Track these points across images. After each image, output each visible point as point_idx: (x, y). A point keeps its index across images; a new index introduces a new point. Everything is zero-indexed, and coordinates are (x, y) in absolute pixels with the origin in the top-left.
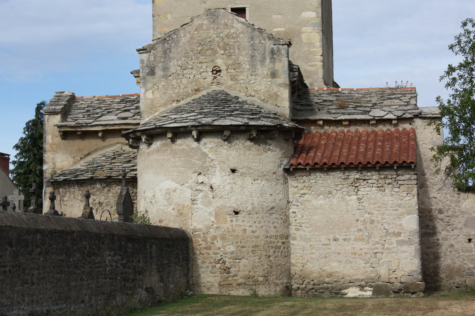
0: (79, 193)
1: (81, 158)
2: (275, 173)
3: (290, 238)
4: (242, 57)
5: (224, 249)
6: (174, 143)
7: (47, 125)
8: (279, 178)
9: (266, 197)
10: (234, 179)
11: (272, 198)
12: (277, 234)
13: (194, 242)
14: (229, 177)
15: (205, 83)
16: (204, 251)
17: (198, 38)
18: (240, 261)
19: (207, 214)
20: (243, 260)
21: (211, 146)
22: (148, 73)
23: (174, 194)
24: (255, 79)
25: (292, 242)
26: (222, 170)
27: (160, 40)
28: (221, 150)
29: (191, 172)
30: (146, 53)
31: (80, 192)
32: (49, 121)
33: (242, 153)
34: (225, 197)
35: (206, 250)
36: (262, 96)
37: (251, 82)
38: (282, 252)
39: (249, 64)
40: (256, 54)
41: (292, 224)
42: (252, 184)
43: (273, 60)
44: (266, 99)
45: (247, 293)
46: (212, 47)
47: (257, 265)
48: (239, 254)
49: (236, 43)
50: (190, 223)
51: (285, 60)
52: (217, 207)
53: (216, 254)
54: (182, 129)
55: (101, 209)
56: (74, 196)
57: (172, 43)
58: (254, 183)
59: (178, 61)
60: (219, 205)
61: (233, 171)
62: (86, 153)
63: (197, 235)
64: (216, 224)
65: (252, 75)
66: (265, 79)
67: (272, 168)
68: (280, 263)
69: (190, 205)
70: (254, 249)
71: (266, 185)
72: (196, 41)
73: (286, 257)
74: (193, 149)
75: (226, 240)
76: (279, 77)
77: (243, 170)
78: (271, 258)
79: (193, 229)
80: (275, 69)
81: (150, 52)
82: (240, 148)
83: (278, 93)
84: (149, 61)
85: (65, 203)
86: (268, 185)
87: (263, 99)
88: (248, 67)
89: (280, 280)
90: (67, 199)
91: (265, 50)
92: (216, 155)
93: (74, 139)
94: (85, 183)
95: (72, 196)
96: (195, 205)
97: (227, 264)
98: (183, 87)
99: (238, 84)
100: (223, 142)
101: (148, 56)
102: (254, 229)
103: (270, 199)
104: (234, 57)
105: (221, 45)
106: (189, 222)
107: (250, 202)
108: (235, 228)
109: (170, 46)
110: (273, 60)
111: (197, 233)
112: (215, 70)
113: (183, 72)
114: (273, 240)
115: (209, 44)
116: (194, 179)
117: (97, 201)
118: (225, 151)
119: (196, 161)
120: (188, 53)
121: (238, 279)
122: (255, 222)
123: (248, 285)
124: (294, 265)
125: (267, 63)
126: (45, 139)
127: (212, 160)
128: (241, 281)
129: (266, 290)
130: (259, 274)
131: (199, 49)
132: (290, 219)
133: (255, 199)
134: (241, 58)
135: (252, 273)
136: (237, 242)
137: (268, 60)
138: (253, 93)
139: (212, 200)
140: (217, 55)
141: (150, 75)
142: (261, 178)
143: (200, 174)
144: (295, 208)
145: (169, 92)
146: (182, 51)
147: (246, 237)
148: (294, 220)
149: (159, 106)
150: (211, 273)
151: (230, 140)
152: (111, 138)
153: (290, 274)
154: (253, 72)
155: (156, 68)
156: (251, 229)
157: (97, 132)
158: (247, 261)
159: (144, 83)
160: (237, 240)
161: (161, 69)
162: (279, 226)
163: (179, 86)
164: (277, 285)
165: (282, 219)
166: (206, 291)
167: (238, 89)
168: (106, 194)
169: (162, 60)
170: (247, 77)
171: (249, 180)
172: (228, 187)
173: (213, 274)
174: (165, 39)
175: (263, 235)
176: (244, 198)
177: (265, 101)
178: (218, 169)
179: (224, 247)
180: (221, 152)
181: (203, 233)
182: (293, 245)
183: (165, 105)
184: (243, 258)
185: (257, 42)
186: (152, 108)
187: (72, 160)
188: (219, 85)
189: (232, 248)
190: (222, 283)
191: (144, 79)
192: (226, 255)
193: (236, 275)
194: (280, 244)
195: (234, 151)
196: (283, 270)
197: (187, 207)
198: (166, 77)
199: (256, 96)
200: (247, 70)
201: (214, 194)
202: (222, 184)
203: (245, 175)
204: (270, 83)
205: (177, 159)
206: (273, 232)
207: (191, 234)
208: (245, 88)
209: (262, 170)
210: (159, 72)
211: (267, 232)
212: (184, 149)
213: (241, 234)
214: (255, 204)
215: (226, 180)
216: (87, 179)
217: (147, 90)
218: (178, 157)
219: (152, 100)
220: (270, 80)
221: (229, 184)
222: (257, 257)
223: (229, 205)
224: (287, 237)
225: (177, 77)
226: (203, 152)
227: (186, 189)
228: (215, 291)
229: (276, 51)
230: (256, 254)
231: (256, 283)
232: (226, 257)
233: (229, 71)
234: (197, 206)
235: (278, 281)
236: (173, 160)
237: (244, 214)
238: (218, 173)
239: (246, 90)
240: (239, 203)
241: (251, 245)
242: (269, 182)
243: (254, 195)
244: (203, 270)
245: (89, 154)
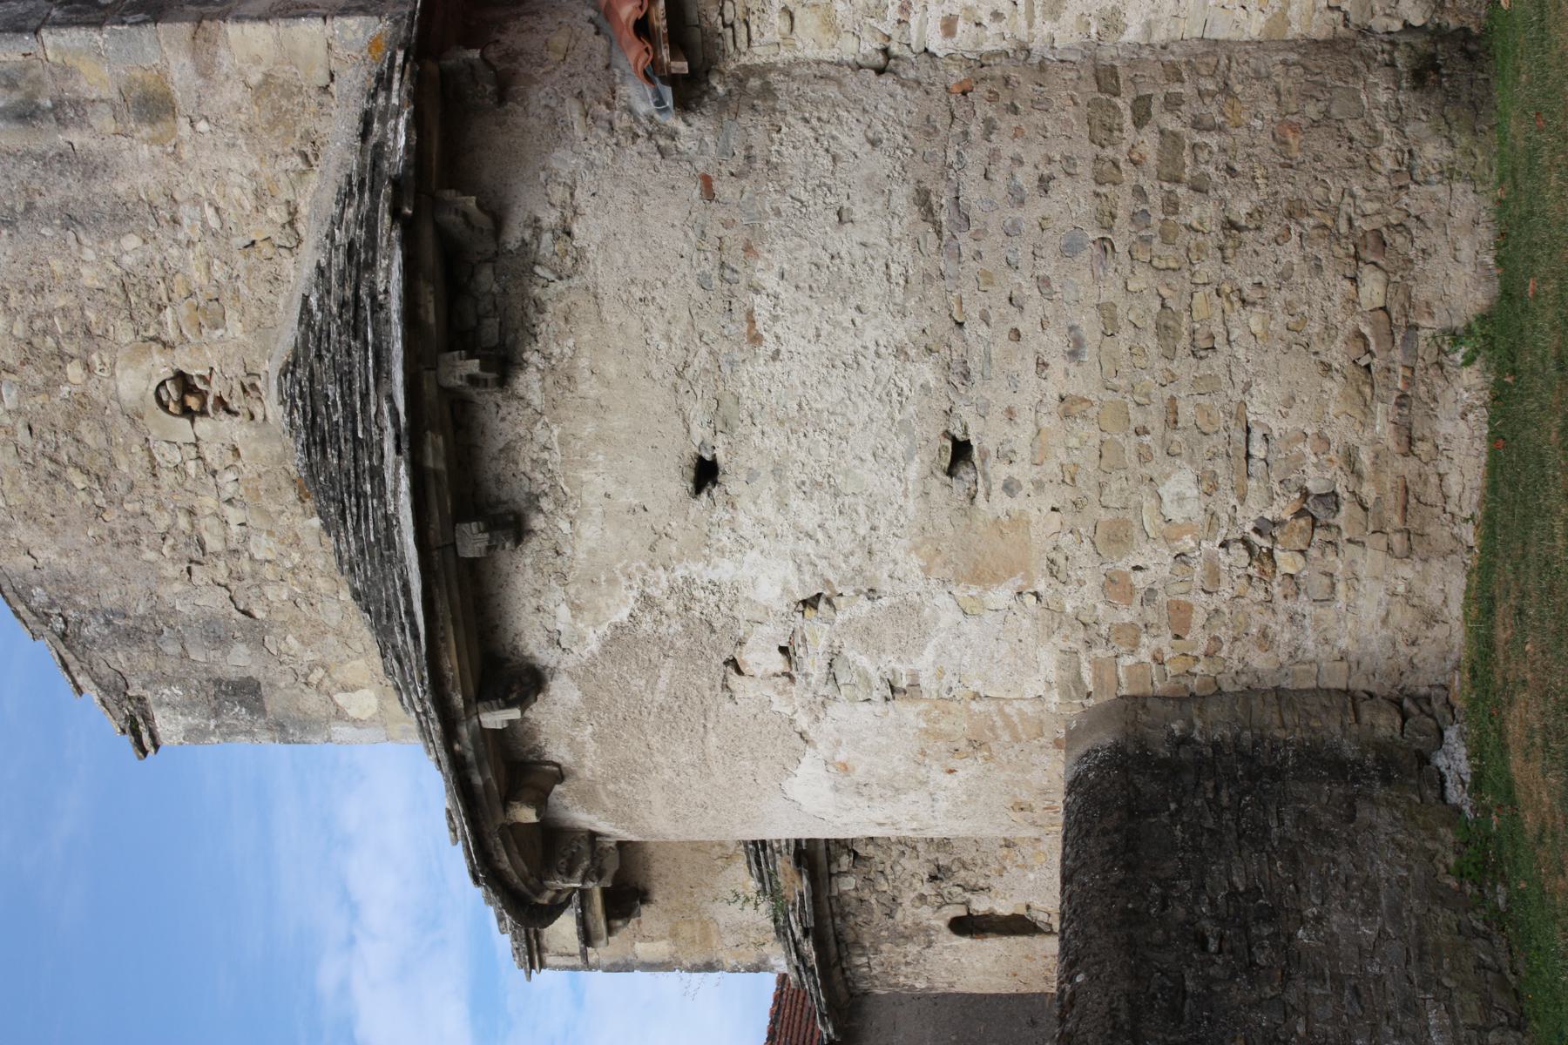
2: (709, 193)
3: (1106, 55)
4: (85, 271)
5: (1182, 530)
8: (740, 153)
9: (858, 252)
10: (752, 475)
11: (859, 212)
12: (1084, 169)
13: (1138, 690)
14: (744, 502)
15: (256, 455)
16: (1198, 639)
17: (25, 486)
18: (1257, 434)
19: (970, 626)
20: (1256, 411)
21: (564, 612)
22: (251, 711)
24: (196, 200)
25: (1132, 34)
26: (703, 545)
27: (69, 657)
28: (581, 556)
29: (729, 706)
30: (148, 719)
33: (589, 429)
34: (863, 530)
35: (1188, 627)
36: (284, 164)
37: (214, 223)
38: (1198, 124)
39: (118, 236)
40: (54, 198)
41: (1023, 34)
42: (776, 355)
43: (68, 110)
44: (295, 143)
45: (1469, 383)
46: (60, 421)
47: (1282, 318)
48: (1218, 442)
49: (12, 303)
50: (1028, 709)
51: (56, 47)
52: (927, 570)
53: (1214, 574)
55: (963, 873)
57: (75, 605)
58: (770, 344)
60: (915, 561)
61: (705, 473)
63: (1097, 677)
64: (1028, 577)
65: (176, 221)
66: (186, 152)
67: (675, 214)
68: (1266, 138)
69: (923, 706)
70: (1185, 341)
71: (779, 260)
72: (41, 499)
73: (1226, 89)
74: (590, 699)
75: (1126, 523)
76: (162, 76)
77: (697, 411)
78: (1241, 209)
79: (1065, 693)
80: (116, 96)
81: (141, 700)
82: (563, 443)
83: (255, 78)
84: (188, 707)
86: (779, 245)
87: (297, 160)
88: (132, 242)
89: (1377, 138)
92: (612, 581)
97: (1282, 509)
98: (296, 556)
99: (236, 290)
100: (533, 544)
101: (167, 712)
102: (1055, 342)
103: (869, 227)
104: (91, 315)
105: (38, 380)
106: (1021, 713)
107: (888, 367)
108: (1052, 467)
109: (93, 612)
110: (68, 110)
111: (1087, 676)
112: (182, 402)
113: (217, 555)
114: (1125, 203)
115: (48, 437)
116: (769, 692)
117: (927, 889)
118: (590, 532)
119: (662, 685)
121: (1375, 441)
122: (1016, 335)
123: (1409, 382)
124: (1282, 18)
125: (94, 144)
127: (647, 601)
128: (1382, 426)
129: (1445, 251)
130: (1348, 300)
131: (79, 481)
132: (987, 47)
133: (870, 335)
134: (89, 277)
135: (1337, 354)
136: (1144, 457)
137: (76, 137)
138: (278, 214)
139: (885, 602)
141: (259, 699)
142: (740, 289)
143: (733, 663)
144: (923, 23)
145: (334, 619)
146: (107, 562)
147: (1108, 396)
148: (993, 28)
150: (1329, 599)
151: (520, 498)
153: (1331, 44)
154: (157, 214)
155: (219, 673)
156: (1058, 365)
158: (1261, 388)
159: (303, 729)
160: (1131, 457)
161: (218, 654)
162: (1034, 154)
163: (294, 570)
164: (1407, 171)
165: (990, 127)
166: (1439, 631)
167: (262, 291)
169: (172, 649)
170: (190, 243)
171: (755, 378)
172: (807, 513)
173: (1341, 587)
174: (63, 636)
175: (1096, 279)
176: (865, 410)
177: (308, 150)
178: (696, 568)
179: (1170, 531)
180: (592, 552)
181: (1089, 644)
182: (1149, 27)
184: (1239, 413)
188: (259, 384)
189: (1180, 484)
190: (1397, 540)
192: (1224, 517)
193: (1350, 459)
194: (1149, 143)
195: (585, 475)
196: (1312, 110)
199: (285, 194)
200: (150, 247)
201: (849, 592)
202: (788, 545)
203: (728, 400)
204: (202, 126)
206: (1072, 202)
207: (1091, 702)
208: (253, 252)
209: (693, 283)
210: (239, 661)
211: (1070, 249)
212: (598, 737)
213: (1090, 432)
214: (900, 335)
215: (760, 522)
217: (340, 715)
220: (183, 123)
221: (783, 506)
222: (1237, 315)
223: (912, 506)
224: (1106, 78)
225: (248, 581)
226: (605, 651)
227: (827, 726)
228: (1448, 586)
229: (16, 96)
230: (1217, 329)
231: (1396, 322)
232: (1233, 520)
233: (171, 334)
234: (923, 675)
235: (1382, 151)
237: (966, 413)
238: (724, 570)
239: (267, 250)
240: (899, 446)
241: (1161, 364)
242: (763, 236)
243: (847, 343)
244: (1310, 644)
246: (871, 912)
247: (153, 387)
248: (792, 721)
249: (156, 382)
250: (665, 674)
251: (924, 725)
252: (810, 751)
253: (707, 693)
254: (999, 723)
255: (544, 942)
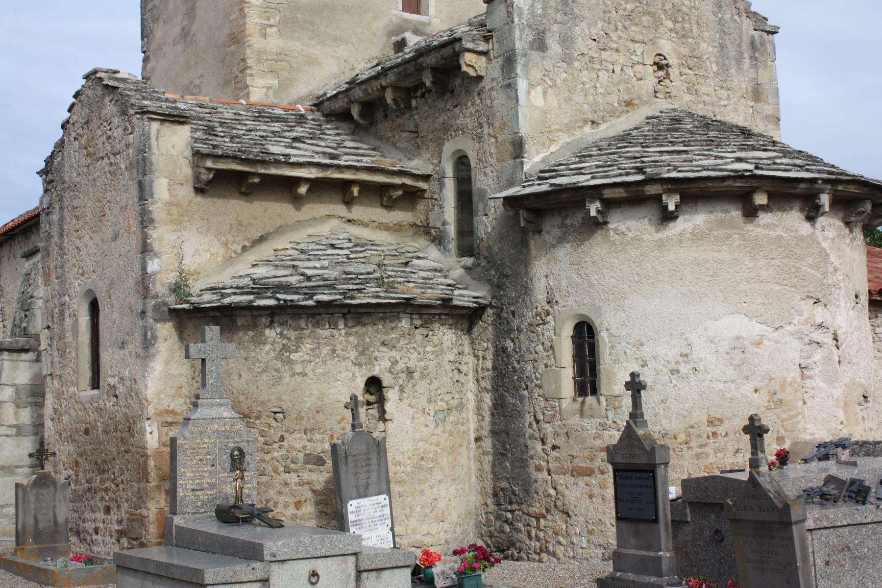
0: (347, 342)
1: (244, 248)
6: (752, 222)
7: (155, 151)
23: (756, 350)
29: (799, 297)
31: (351, 339)
32: (161, 140)
39: (717, 63)
40: (728, 43)
49: (693, 10)
50: (800, 426)
54: (803, 186)
55: (410, 385)
56: (334, 351)
59: (589, 26)
62: (257, 235)
74: (802, 239)
84: (533, 14)
85: (298, 369)
88: (715, 68)
90: (306, 357)
91: (740, 37)
93: (225, 197)
94: (369, 314)
95: (326, 350)
96: (808, 381)
98: (601, 91)
106: (798, 423)
116: (806, 316)
117: (401, 366)
119: (809, 270)
120: (610, 12)
126: (151, 186)
134: (703, 45)
137: (747, 61)
140: (661, 30)
149: (559, 130)
152: (313, 202)
155: (548, 35)
157: (298, 181)
163: (595, 87)
168: (421, 346)
183: (568, 128)
185: (727, 17)
186: (547, 134)
187: (222, 251)
191: (525, 55)
197: (791, 385)
198: (567, 59)
205: (763, 262)
210: (555, 48)
212: (780, 238)
216: (397, 303)
218: (766, 258)
219: (545, 112)
220: (752, 104)
229: (758, 45)
234: (812, 381)
236: (751, 265)
245: (262, 239)
246: (386, 333)
247: (665, 54)
248: (790, 323)
249: (667, 57)
250: (814, 272)
251: (788, 380)
252: (771, 329)
253: (806, 289)
254: (792, 413)
255: (167, 124)
